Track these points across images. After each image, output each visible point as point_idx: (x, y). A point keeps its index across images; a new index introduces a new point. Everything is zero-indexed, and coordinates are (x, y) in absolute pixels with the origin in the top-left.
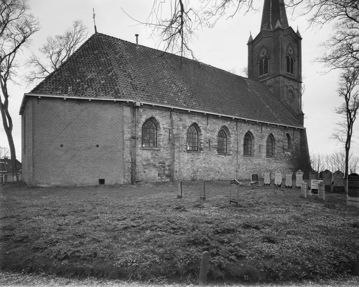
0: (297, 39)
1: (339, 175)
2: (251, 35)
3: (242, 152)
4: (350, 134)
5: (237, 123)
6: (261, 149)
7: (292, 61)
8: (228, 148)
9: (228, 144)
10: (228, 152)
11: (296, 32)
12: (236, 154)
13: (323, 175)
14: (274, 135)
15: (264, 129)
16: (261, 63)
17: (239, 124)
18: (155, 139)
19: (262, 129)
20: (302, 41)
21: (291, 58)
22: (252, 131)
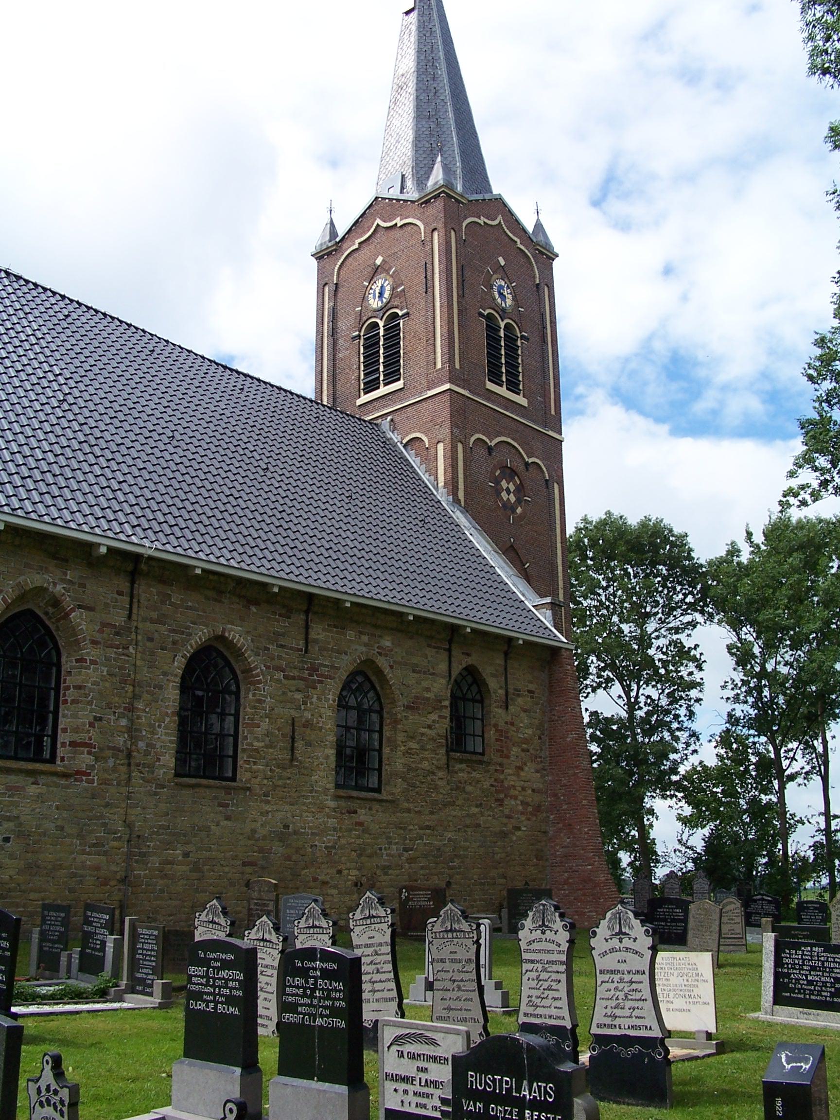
0: (827, 742)
1: (627, 942)
2: (331, 219)
3: (169, 760)
4: (553, 413)
5: (133, 582)
6: (299, 744)
7: (511, 340)
8: (65, 730)
9: (66, 702)
10: (61, 752)
11: (530, 228)
12: (114, 769)
13: (523, 945)
14: (387, 671)
15: (318, 632)
16: (371, 344)
17: (147, 592)
18: (372, 753)
19: (307, 627)
20: (556, 264)
21: (508, 327)
22: (236, 634)
